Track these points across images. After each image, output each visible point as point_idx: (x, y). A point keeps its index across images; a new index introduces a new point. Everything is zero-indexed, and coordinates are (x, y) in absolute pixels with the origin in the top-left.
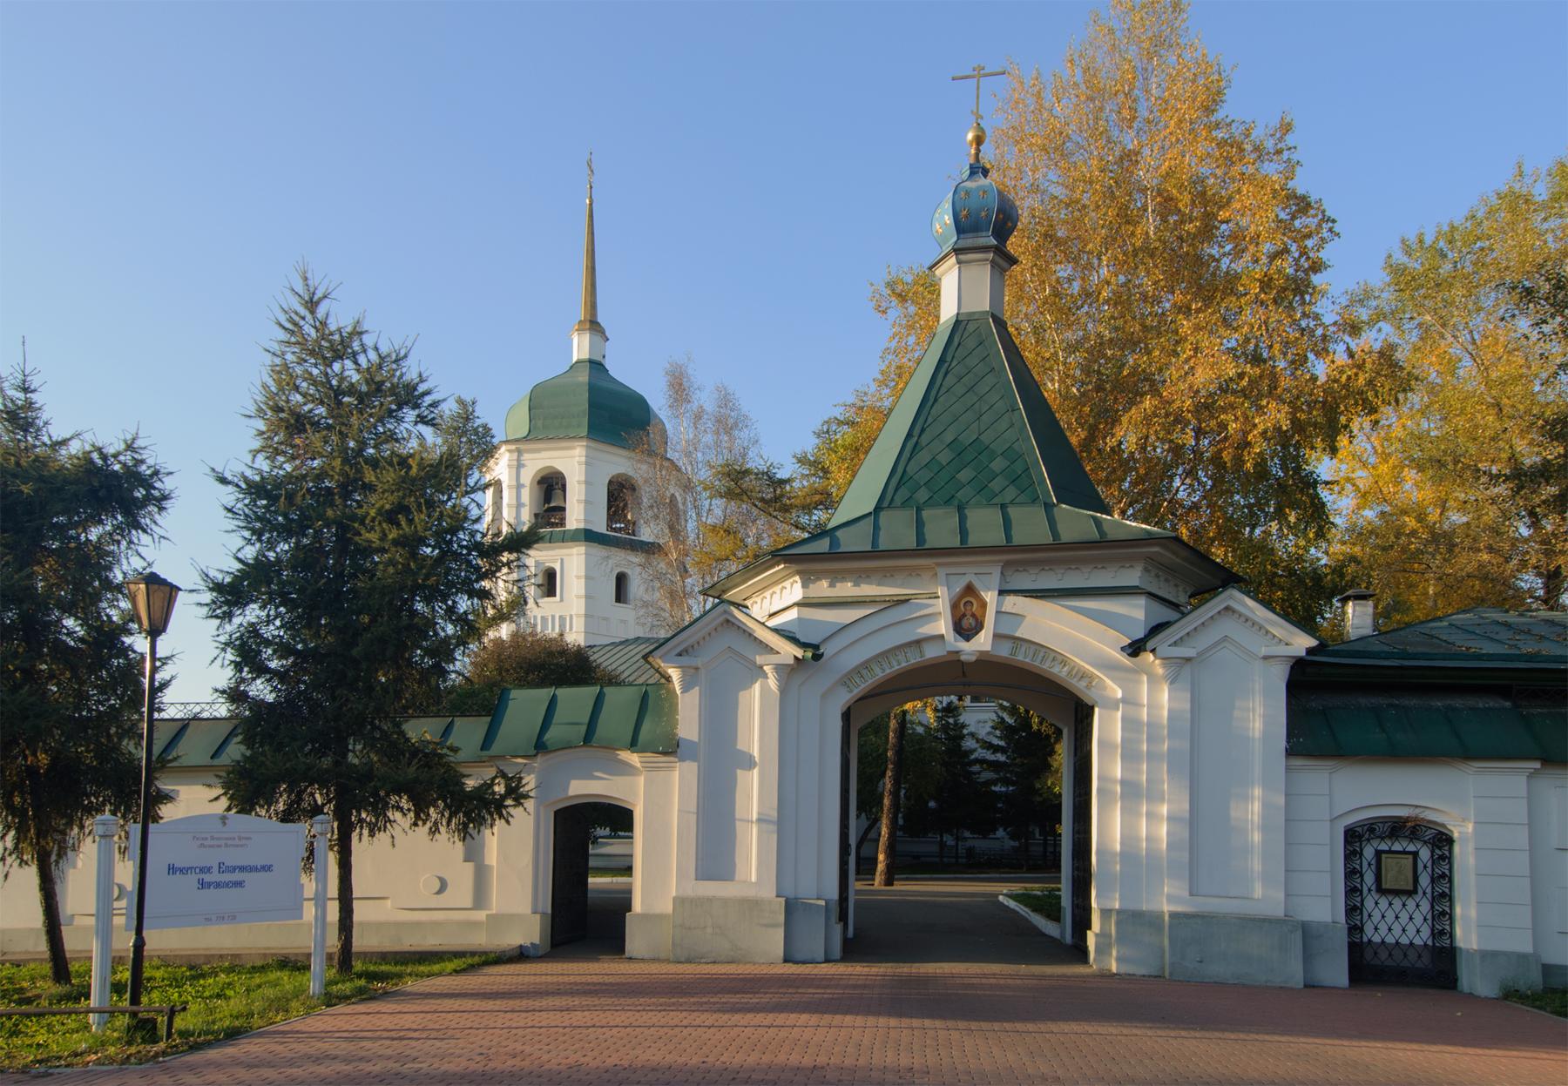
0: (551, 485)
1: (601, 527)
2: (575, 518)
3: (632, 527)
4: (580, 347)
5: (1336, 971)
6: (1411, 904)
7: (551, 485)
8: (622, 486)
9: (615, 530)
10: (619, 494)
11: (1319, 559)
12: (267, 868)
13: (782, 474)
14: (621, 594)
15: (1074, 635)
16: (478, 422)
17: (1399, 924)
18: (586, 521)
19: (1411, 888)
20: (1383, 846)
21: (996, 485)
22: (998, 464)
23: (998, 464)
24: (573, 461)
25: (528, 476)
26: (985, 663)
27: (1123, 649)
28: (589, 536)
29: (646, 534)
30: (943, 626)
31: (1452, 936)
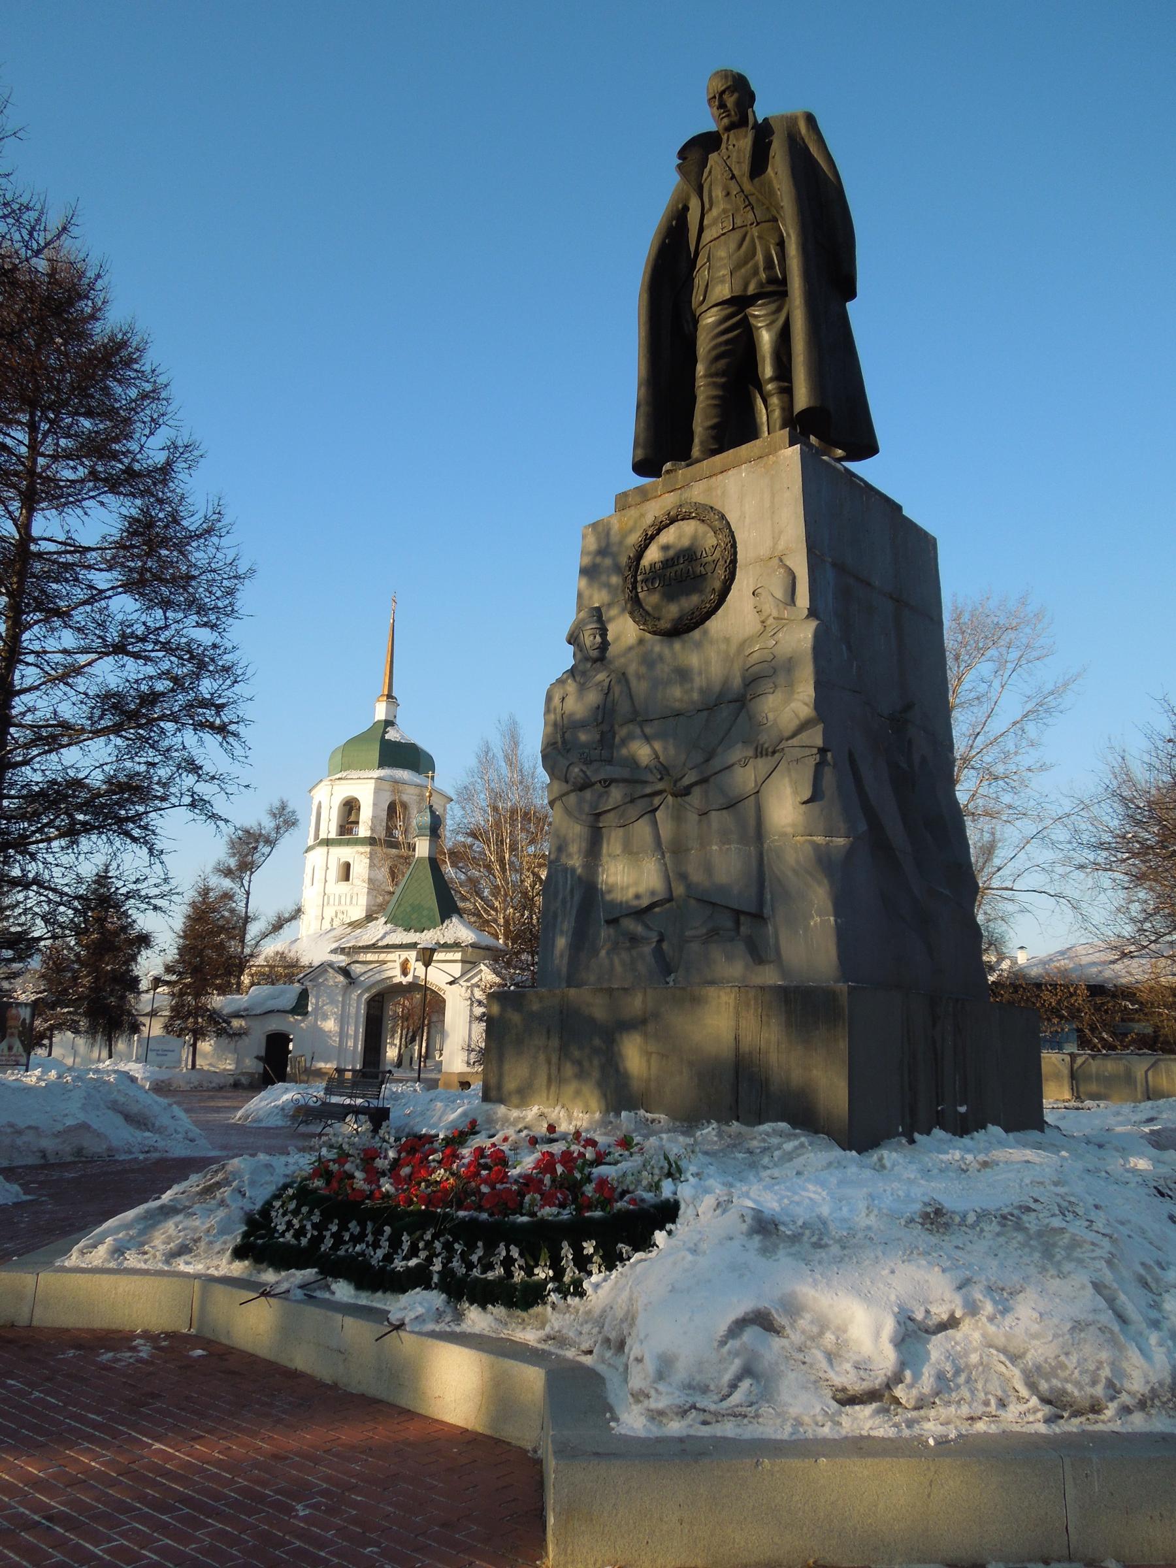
0: (350, 807)
2: (363, 831)
4: (381, 712)
7: (350, 807)
22: (425, 913)
23: (425, 913)
24: (365, 787)
26: (410, 984)
30: (397, 972)
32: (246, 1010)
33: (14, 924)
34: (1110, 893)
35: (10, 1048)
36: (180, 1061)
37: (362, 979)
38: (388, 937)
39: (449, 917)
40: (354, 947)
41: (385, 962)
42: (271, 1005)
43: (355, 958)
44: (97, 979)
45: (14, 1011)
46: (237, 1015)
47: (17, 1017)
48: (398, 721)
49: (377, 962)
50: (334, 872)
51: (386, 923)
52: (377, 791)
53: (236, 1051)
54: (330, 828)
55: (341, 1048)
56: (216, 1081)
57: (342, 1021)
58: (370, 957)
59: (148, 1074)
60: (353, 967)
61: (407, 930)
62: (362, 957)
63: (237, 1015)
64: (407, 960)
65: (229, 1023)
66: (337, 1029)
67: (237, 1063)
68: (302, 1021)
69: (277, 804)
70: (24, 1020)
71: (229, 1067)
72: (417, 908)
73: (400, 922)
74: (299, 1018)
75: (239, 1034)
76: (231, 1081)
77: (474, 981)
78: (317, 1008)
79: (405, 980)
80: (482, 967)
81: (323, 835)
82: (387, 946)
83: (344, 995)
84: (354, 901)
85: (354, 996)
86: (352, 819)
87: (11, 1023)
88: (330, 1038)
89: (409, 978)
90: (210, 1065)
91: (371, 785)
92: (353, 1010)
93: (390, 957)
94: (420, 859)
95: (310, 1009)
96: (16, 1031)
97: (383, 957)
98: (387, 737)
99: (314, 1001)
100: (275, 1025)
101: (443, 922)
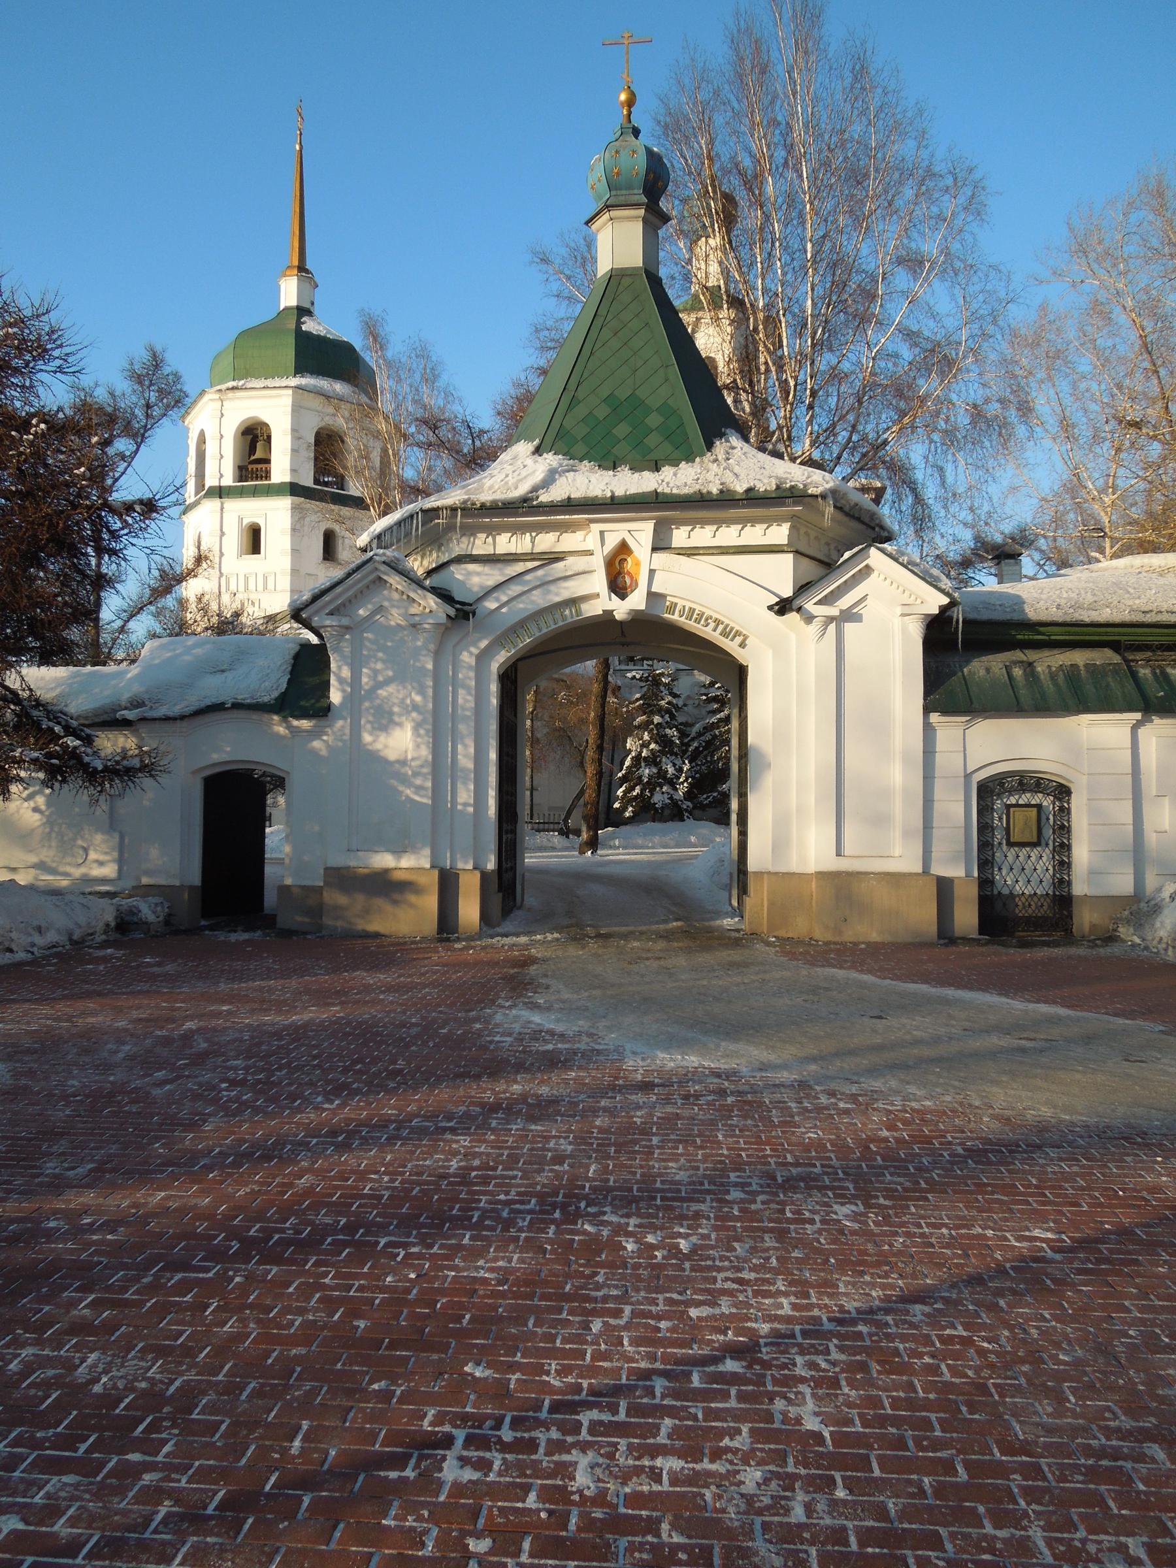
0: (254, 437)
1: (308, 481)
2: (281, 470)
3: (341, 483)
4: (289, 293)
5: (966, 917)
6: (1034, 853)
7: (254, 437)
8: (329, 436)
9: (326, 484)
10: (326, 447)
11: (274, 962)
13: (478, 425)
15: (723, 584)
16: (167, 370)
17: (1025, 875)
18: (293, 471)
19: (1035, 840)
20: (1013, 800)
21: (653, 440)
22: (654, 420)
23: (654, 420)
24: (275, 404)
25: (231, 428)
26: (638, 620)
27: (770, 608)
28: (294, 489)
29: (354, 488)
30: (598, 582)
31: (1069, 883)
32: (136, 703)
37: (491, 605)
39: (721, 435)
41: (554, 558)
42: (215, 688)
43: (459, 546)
46: (112, 721)
48: (316, 310)
50: (234, 540)
51: (538, 451)
52: (297, 409)
53: (112, 825)
54: (222, 467)
55: (440, 807)
56: (58, 925)
57: (439, 729)
58: (505, 543)
60: (458, 572)
61: (611, 463)
62: (481, 545)
63: (112, 721)
64: (623, 548)
65: (88, 741)
66: (425, 752)
67: (121, 861)
68: (315, 734)
69: (142, 356)
71: (97, 872)
72: (628, 408)
73: (581, 448)
74: (305, 724)
75: (121, 772)
76: (107, 913)
77: (845, 602)
79: (621, 609)
81: (211, 481)
82: (570, 505)
83: (437, 655)
84: (271, 586)
85: (467, 658)
86: (259, 454)
88: (405, 780)
89: (637, 600)
90: (41, 866)
91: (285, 400)
92: (466, 699)
93: (570, 541)
95: (335, 697)
97: (546, 542)
98: (304, 328)
99: (346, 673)
100: (227, 746)
101: (710, 446)
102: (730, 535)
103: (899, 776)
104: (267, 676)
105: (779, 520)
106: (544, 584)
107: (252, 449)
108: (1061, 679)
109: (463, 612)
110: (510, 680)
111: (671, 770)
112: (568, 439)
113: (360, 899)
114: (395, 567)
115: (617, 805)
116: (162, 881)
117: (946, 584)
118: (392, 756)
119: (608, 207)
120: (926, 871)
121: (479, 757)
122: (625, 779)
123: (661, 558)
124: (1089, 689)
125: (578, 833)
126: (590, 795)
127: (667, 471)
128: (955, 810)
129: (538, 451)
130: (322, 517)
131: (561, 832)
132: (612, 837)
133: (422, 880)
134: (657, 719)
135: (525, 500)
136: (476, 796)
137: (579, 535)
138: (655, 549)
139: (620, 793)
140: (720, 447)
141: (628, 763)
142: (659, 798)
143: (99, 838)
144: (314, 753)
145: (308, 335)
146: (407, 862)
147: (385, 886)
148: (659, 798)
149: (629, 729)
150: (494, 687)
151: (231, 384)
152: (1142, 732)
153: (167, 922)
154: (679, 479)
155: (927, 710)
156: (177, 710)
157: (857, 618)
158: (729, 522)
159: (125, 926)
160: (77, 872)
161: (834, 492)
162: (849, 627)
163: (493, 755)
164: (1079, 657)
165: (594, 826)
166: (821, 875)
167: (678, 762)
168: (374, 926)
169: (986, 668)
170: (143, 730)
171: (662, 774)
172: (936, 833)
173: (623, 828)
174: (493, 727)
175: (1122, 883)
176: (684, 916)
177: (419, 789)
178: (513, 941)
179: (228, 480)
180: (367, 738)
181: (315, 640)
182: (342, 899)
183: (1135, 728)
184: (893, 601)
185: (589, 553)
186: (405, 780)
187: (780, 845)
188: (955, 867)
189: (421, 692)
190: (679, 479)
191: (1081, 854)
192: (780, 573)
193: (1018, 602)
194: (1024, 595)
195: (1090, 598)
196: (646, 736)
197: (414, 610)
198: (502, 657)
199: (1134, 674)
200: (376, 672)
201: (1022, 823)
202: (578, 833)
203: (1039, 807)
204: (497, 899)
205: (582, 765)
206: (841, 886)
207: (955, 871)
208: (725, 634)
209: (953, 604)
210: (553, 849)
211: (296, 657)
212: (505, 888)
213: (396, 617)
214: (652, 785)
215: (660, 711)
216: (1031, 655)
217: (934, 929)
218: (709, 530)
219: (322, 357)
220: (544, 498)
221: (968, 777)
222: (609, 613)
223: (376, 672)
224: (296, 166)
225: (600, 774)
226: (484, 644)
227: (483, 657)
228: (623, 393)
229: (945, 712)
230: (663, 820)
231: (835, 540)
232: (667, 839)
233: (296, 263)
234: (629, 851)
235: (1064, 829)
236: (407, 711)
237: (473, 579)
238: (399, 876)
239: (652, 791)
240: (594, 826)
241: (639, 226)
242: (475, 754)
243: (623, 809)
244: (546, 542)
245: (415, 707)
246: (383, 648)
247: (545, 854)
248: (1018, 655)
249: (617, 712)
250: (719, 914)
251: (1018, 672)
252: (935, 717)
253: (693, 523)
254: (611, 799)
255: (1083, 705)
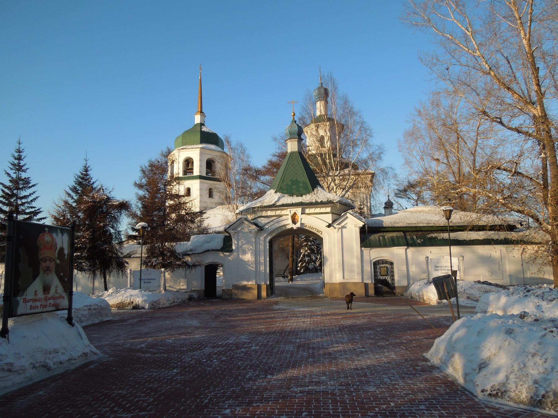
0: (188, 162)
1: (204, 174)
3: (213, 173)
4: (198, 119)
5: (372, 292)
7: (188, 162)
10: (210, 164)
12: (154, 279)
14: (211, 195)
15: (316, 221)
18: (200, 172)
21: (301, 189)
22: (301, 185)
23: (301, 185)
24: (195, 153)
26: (298, 229)
28: (201, 177)
30: (290, 221)
32: (191, 250)
33: (29, 207)
34: (526, 185)
35: (46, 289)
36: (159, 286)
38: (281, 200)
39: (316, 187)
40: (261, 207)
41: (281, 216)
44: (93, 232)
45: (47, 238)
47: (53, 246)
49: (275, 216)
51: (276, 192)
52: (201, 154)
53: (185, 277)
55: (257, 271)
57: (256, 254)
58: (269, 213)
59: (145, 298)
60: (260, 220)
61: (292, 195)
62: (264, 214)
66: (253, 259)
67: (187, 285)
70: (62, 249)
71: (182, 287)
72: (295, 182)
73: (285, 191)
74: (227, 254)
77: (343, 224)
78: (237, 248)
79: (295, 227)
80: (348, 215)
82: (283, 205)
83: (255, 238)
85: (262, 238)
86: (190, 167)
87: (44, 254)
88: (249, 265)
89: (298, 225)
91: (198, 151)
92: (262, 247)
93: (284, 212)
94: (292, 153)
95: (234, 247)
96: (52, 265)
97: (278, 213)
99: (236, 242)
100: (210, 259)
101: (313, 190)
102: (318, 210)
103: (356, 262)
104: (218, 243)
105: (328, 207)
106: (278, 222)
107: (188, 165)
108: (390, 240)
109: (261, 229)
110: (271, 242)
111: (314, 258)
112: (283, 189)
113: (240, 291)
114: (246, 219)
115: (299, 269)
116: (197, 289)
117: (364, 220)
118: (246, 260)
119: (290, 139)
120: (362, 282)
121: (265, 260)
122: (301, 261)
123: (303, 215)
124: (396, 242)
125: (287, 277)
126: (290, 266)
127: (304, 196)
128: (368, 268)
129: (276, 192)
130: (209, 184)
131: (283, 277)
132: (297, 278)
133: (253, 287)
134: (309, 243)
135: (274, 205)
136: (264, 268)
137: (285, 211)
138: (302, 214)
139: (299, 265)
140: (315, 190)
141: (302, 256)
142: (311, 266)
143: (182, 280)
144: (229, 260)
145: (204, 132)
146: (250, 283)
147: (246, 288)
148: (311, 266)
149: (301, 247)
150: (268, 244)
151: (182, 147)
152: (408, 250)
153: (198, 298)
154: (307, 198)
155: (361, 247)
156: (200, 251)
157: (345, 228)
158: (318, 208)
159: (191, 299)
160: (178, 288)
161: (339, 201)
162: (344, 229)
163: (268, 259)
164: (394, 234)
165: (292, 275)
166: (340, 283)
167: (316, 256)
168: (243, 297)
169: (374, 237)
170: (192, 256)
171: (311, 259)
172: (364, 273)
173: (301, 276)
174: (268, 253)
175: (405, 283)
176: (311, 293)
177: (252, 267)
178: (273, 299)
179: (181, 175)
180: (241, 256)
181: (227, 234)
182: (236, 292)
183: (406, 250)
184: (353, 224)
185: (288, 215)
186: (249, 265)
187: (331, 277)
188: (369, 281)
189: (252, 246)
190: (307, 198)
191: (396, 277)
192: (329, 218)
193: (382, 222)
194: (384, 220)
195: (398, 220)
196: (306, 249)
197: (250, 228)
198: (269, 238)
199: (406, 238)
200: (242, 242)
201: (383, 271)
202: (287, 277)
203: (387, 267)
204: (270, 291)
205: (288, 258)
206: (343, 285)
207: (368, 281)
208: (317, 231)
209: (365, 224)
210: (281, 282)
211: (224, 239)
212: (271, 289)
213: (246, 230)
214: (308, 263)
215: (310, 241)
216: (385, 234)
217: (364, 294)
218: (313, 209)
219: (209, 138)
220: (278, 204)
221: (371, 261)
222: (292, 228)
223: (242, 242)
224: (199, 83)
225: (293, 260)
226: (265, 235)
227: (265, 238)
228: (294, 179)
229: (365, 247)
230: (312, 273)
231: (340, 210)
232: (313, 278)
233: (200, 110)
234: (300, 281)
235: (393, 272)
236: (249, 250)
237: (263, 221)
238: (248, 286)
239: (309, 264)
240: (292, 275)
241: (297, 143)
242: (264, 259)
243: (301, 269)
244: (278, 213)
245: (251, 249)
246: (244, 237)
247: (280, 282)
248: (382, 234)
249: (298, 243)
250: (320, 293)
251: (381, 238)
252: (363, 248)
253: (310, 208)
254: (297, 267)
255: (394, 245)
